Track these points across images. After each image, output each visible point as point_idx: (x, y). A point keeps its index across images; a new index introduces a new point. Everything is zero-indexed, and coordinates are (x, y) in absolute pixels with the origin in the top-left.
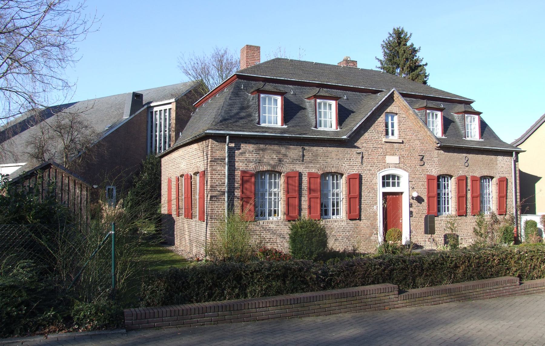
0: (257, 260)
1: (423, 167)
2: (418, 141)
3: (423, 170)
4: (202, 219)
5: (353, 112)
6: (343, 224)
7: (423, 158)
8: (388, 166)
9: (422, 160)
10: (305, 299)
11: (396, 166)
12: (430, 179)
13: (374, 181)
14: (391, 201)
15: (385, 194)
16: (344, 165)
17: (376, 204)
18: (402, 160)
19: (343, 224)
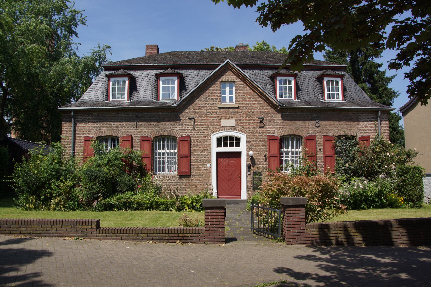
0: (275, 205)
1: (263, 129)
2: (258, 105)
3: (263, 132)
4: (390, 105)
5: (304, 30)
6: (174, 179)
7: (262, 120)
8: (224, 128)
9: (261, 122)
10: (110, 231)
11: (232, 128)
12: (272, 139)
13: (207, 142)
14: (229, 160)
15: (220, 155)
16: (176, 129)
17: (210, 162)
18: (239, 122)
19: (174, 179)
